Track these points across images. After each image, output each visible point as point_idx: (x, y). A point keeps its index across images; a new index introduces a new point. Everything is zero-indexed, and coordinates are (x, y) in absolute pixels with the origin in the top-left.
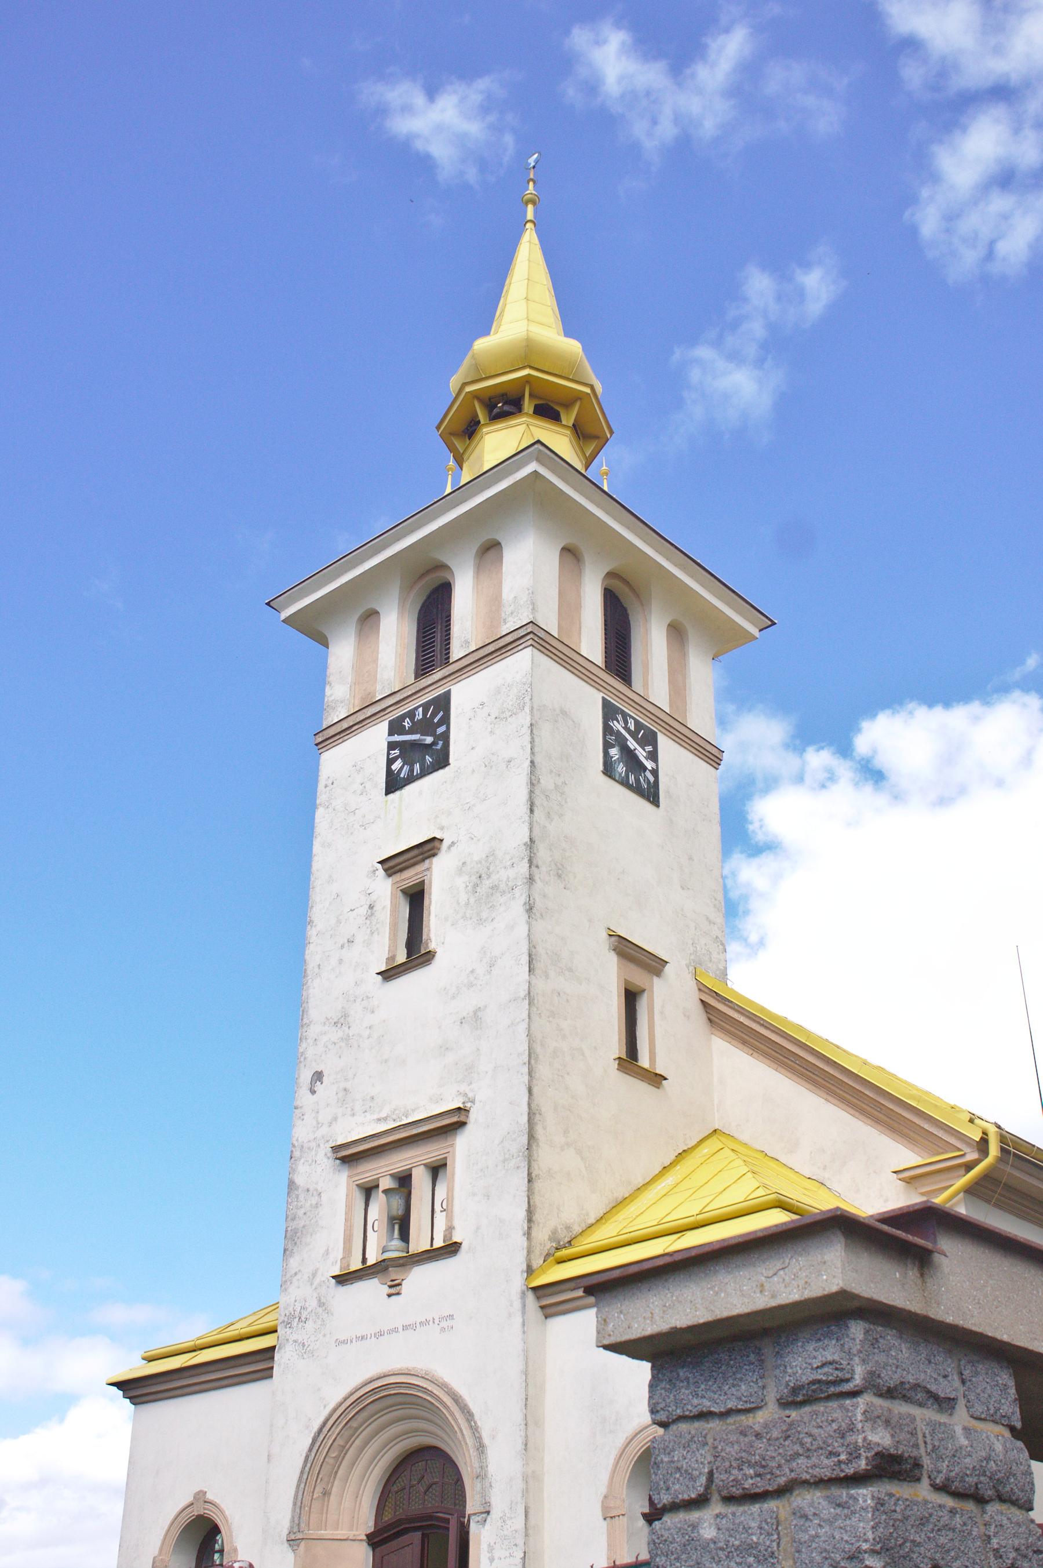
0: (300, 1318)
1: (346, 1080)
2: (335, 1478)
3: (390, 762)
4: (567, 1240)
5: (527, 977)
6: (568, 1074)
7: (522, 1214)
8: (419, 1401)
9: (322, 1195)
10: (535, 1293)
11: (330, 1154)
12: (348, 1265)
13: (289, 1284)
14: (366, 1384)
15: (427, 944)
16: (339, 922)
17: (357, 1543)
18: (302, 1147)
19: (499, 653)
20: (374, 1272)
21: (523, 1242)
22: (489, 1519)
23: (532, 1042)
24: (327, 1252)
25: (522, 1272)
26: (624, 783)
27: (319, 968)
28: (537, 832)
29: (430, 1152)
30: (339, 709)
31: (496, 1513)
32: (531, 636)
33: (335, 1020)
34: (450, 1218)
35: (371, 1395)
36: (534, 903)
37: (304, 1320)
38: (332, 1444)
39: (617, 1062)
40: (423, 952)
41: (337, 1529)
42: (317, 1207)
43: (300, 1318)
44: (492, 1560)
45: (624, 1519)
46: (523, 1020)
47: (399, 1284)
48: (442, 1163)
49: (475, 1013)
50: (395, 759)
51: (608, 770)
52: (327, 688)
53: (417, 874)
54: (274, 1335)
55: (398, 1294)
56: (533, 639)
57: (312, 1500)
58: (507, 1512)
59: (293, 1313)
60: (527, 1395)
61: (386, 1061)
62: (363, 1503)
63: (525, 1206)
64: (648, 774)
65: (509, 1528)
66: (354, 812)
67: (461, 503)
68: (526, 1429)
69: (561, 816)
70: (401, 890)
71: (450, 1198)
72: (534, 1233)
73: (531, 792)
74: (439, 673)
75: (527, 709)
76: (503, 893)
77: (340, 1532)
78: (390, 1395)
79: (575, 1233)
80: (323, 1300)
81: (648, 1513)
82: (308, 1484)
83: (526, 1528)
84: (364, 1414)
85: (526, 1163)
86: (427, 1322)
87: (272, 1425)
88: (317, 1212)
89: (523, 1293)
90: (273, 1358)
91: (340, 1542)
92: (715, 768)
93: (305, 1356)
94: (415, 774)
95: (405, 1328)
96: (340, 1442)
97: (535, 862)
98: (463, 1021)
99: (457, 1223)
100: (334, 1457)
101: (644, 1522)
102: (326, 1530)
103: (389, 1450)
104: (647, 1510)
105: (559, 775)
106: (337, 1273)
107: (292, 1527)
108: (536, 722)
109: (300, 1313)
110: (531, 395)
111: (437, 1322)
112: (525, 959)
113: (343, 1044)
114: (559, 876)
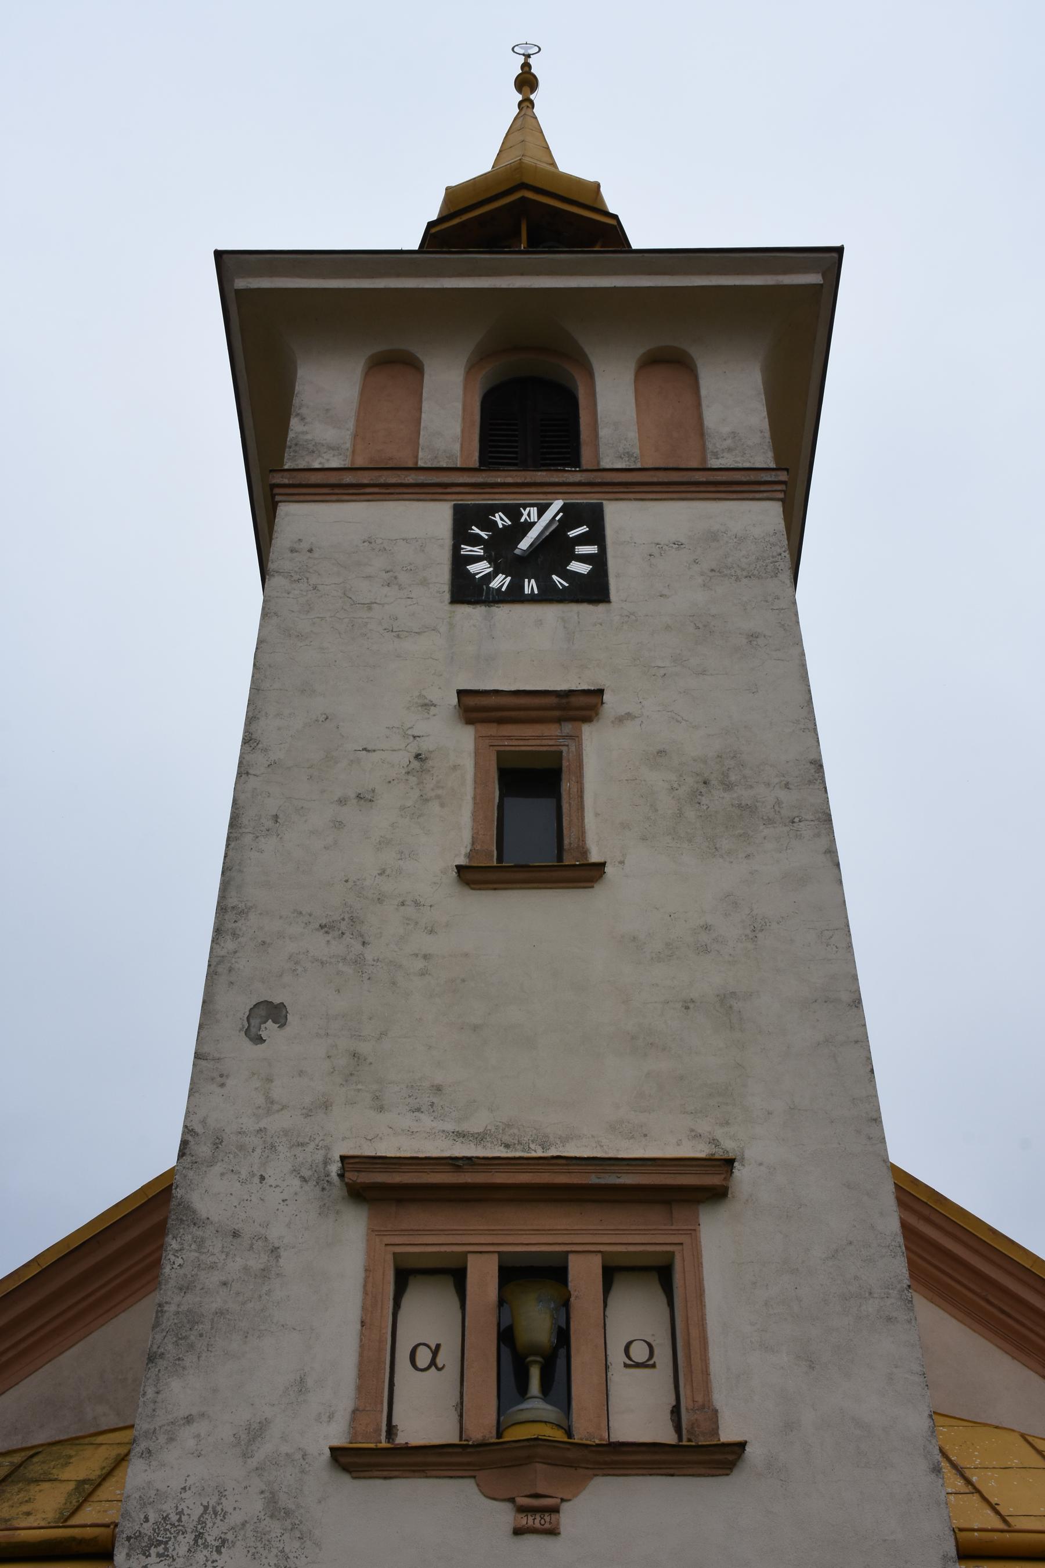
0: (199, 1536)
13: (162, 1439)
20: (469, 1464)
43: (199, 1536)
47: (555, 1510)
52: (294, 422)
59: (174, 1518)
70: (498, 752)
109: (201, 1521)
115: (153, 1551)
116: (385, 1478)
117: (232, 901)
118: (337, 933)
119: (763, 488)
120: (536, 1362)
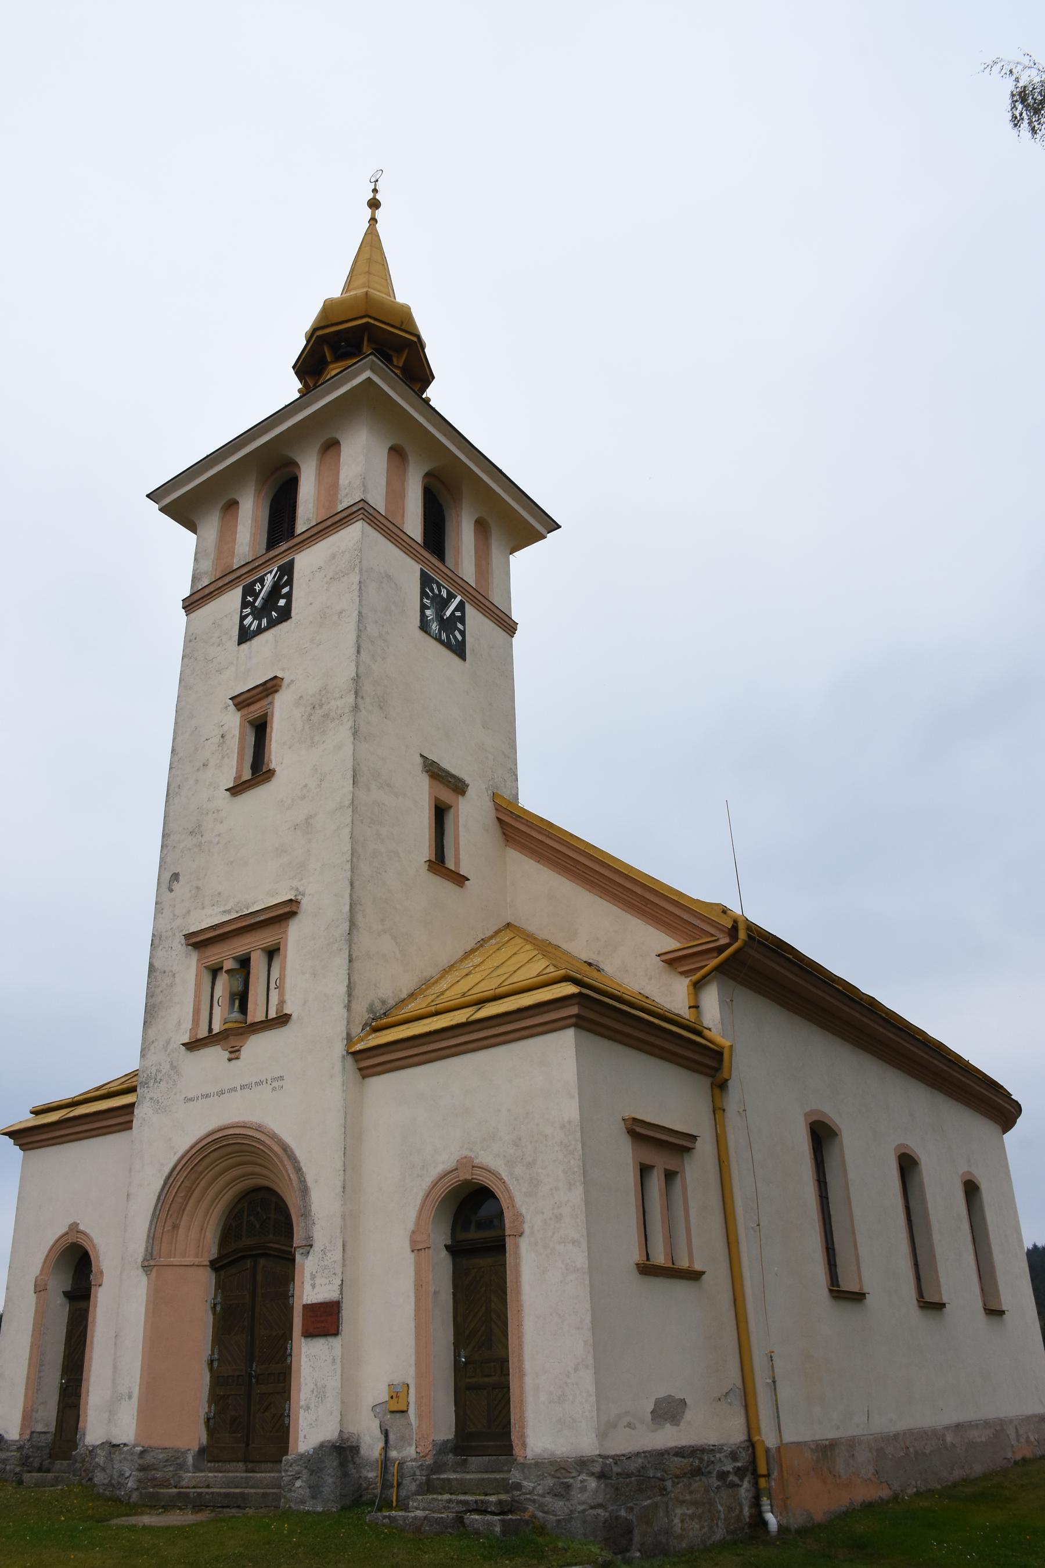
0: (156, 1079)
1: (199, 879)
3: (243, 618)
4: (382, 1012)
5: (352, 789)
6: (385, 872)
7: (343, 989)
8: (253, 1149)
9: (176, 975)
10: (354, 1057)
11: (183, 941)
12: (196, 1034)
13: (147, 1050)
14: (209, 1135)
15: (268, 765)
16: (196, 750)
17: (201, 1269)
18: (161, 936)
19: (335, 527)
21: (344, 1013)
22: (312, 1251)
23: (354, 843)
24: (179, 1024)
25: (343, 1039)
26: (439, 640)
27: (179, 788)
28: (362, 669)
29: (265, 938)
30: (203, 579)
31: (318, 1246)
32: (362, 511)
33: (191, 830)
34: (282, 995)
36: (359, 727)
37: (158, 1080)
39: (428, 863)
40: (264, 770)
41: (184, 1256)
42: (172, 986)
44: (313, 1286)
45: (431, 1251)
46: (347, 825)
47: (239, 1050)
48: (276, 947)
49: (307, 819)
50: (247, 616)
51: (424, 626)
53: (261, 708)
54: (134, 1094)
55: (237, 1058)
56: (364, 514)
57: (163, 1233)
58: (327, 1245)
60: (345, 1145)
61: (232, 863)
62: (207, 1233)
63: (346, 983)
64: (457, 633)
65: (329, 1259)
66: (212, 661)
67: (307, 407)
68: (345, 1174)
69: (384, 659)
70: (248, 722)
71: (282, 977)
72: (353, 1006)
73: (358, 637)
74: (285, 545)
75: (357, 570)
76: (333, 720)
77: (187, 1259)
78: (229, 1144)
79: (389, 1006)
80: (175, 1064)
81: (451, 1245)
82: (159, 1220)
83: (343, 1259)
85: (347, 946)
86: (261, 1082)
87: (130, 1169)
89: (343, 1057)
90: (133, 1113)
92: (511, 636)
93: (159, 1111)
94: (263, 627)
95: (242, 1087)
96: (187, 1183)
97: (360, 694)
98: (297, 827)
99: (288, 997)
100: (182, 1197)
101: (446, 1252)
102: (175, 1258)
103: (229, 1189)
104: (449, 1242)
105: (383, 626)
106: (186, 1040)
107: (146, 1255)
108: (364, 580)
110: (369, 340)
112: (350, 774)
113: (196, 850)
114: (381, 708)
115: (146, 1086)
116: (198, 1050)
117: (166, 831)
118: (194, 834)
119: (354, 516)
120: (237, 998)
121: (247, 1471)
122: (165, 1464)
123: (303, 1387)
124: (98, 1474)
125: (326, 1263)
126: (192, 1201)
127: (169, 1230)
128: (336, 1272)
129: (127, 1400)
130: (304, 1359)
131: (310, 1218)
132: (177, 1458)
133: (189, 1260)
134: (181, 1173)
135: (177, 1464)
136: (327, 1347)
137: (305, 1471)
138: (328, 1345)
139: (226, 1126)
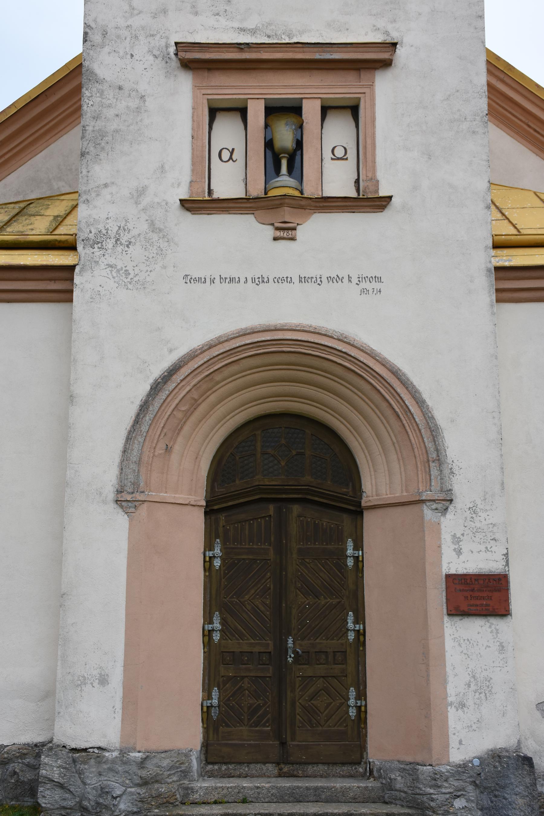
0: (118, 240)
2: (178, 434)
22: (451, 508)
35: (252, 348)
38: (185, 396)
43: (118, 240)
44: (459, 552)
47: (294, 229)
65: (483, 520)
84: (234, 368)
88: (139, 118)
91: (181, 506)
95: (301, 280)
96: (195, 394)
111: (355, 280)
121: (281, 775)
122: (169, 773)
123: (450, 678)
124: (48, 792)
125: (478, 525)
126: (193, 418)
127: (160, 454)
128: (497, 536)
129: (96, 684)
130: (449, 644)
131: (446, 465)
132: (182, 763)
133: (182, 498)
134: (189, 378)
135: (181, 771)
136: (490, 630)
137: (470, 788)
138: (490, 627)
139: (278, 327)
